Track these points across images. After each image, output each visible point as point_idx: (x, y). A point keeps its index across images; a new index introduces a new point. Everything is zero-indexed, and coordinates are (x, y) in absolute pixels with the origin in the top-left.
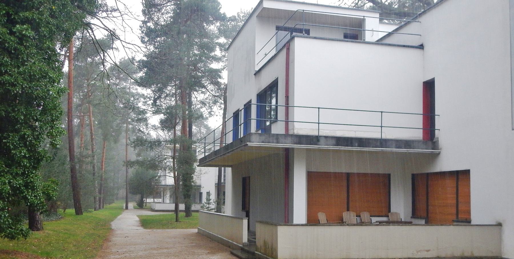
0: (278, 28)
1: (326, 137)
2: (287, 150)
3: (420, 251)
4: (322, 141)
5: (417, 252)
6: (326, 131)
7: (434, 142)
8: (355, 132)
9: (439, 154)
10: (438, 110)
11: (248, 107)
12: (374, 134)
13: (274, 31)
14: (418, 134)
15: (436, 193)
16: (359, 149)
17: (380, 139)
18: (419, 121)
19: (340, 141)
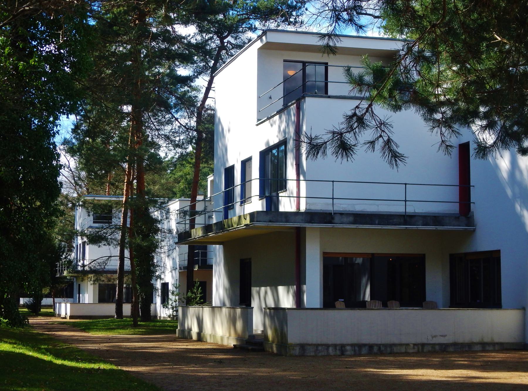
0: (285, 61)
1: (341, 214)
2: (298, 229)
3: (435, 336)
4: (337, 219)
5: (433, 337)
6: (341, 206)
7: (469, 218)
8: (378, 206)
9: (474, 230)
10: (473, 180)
11: (246, 163)
12: (398, 208)
13: (282, 64)
14: (455, 208)
15: (477, 280)
16: (379, 227)
17: (404, 216)
18: (454, 194)
19: (360, 218)
